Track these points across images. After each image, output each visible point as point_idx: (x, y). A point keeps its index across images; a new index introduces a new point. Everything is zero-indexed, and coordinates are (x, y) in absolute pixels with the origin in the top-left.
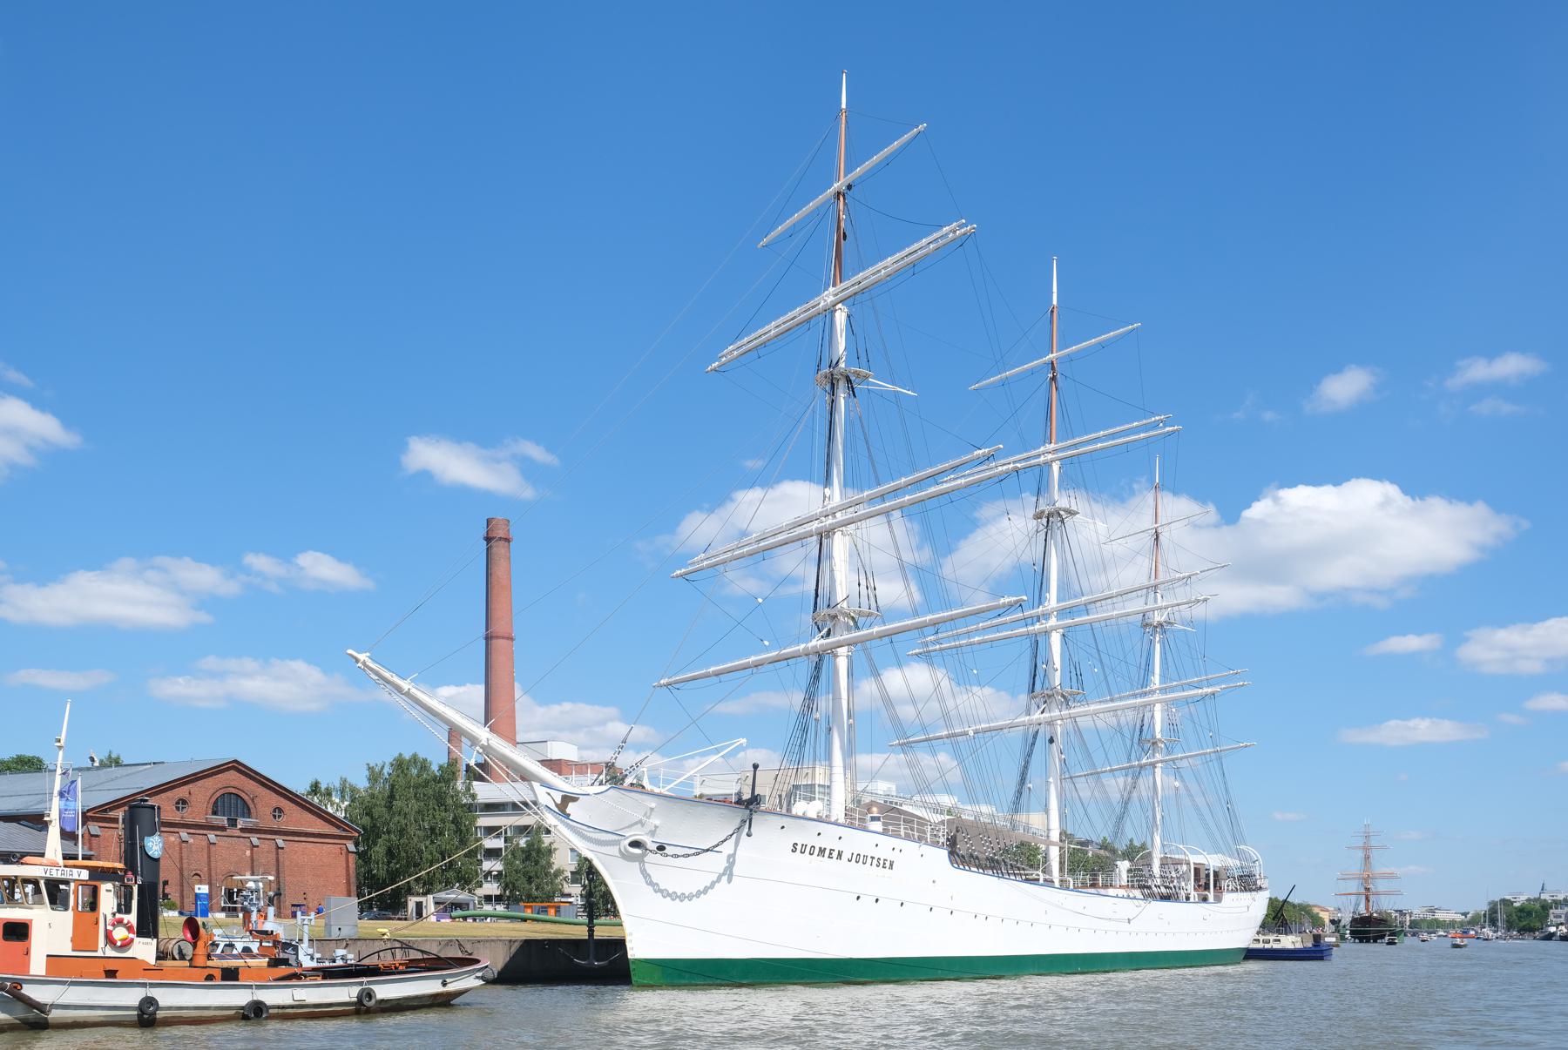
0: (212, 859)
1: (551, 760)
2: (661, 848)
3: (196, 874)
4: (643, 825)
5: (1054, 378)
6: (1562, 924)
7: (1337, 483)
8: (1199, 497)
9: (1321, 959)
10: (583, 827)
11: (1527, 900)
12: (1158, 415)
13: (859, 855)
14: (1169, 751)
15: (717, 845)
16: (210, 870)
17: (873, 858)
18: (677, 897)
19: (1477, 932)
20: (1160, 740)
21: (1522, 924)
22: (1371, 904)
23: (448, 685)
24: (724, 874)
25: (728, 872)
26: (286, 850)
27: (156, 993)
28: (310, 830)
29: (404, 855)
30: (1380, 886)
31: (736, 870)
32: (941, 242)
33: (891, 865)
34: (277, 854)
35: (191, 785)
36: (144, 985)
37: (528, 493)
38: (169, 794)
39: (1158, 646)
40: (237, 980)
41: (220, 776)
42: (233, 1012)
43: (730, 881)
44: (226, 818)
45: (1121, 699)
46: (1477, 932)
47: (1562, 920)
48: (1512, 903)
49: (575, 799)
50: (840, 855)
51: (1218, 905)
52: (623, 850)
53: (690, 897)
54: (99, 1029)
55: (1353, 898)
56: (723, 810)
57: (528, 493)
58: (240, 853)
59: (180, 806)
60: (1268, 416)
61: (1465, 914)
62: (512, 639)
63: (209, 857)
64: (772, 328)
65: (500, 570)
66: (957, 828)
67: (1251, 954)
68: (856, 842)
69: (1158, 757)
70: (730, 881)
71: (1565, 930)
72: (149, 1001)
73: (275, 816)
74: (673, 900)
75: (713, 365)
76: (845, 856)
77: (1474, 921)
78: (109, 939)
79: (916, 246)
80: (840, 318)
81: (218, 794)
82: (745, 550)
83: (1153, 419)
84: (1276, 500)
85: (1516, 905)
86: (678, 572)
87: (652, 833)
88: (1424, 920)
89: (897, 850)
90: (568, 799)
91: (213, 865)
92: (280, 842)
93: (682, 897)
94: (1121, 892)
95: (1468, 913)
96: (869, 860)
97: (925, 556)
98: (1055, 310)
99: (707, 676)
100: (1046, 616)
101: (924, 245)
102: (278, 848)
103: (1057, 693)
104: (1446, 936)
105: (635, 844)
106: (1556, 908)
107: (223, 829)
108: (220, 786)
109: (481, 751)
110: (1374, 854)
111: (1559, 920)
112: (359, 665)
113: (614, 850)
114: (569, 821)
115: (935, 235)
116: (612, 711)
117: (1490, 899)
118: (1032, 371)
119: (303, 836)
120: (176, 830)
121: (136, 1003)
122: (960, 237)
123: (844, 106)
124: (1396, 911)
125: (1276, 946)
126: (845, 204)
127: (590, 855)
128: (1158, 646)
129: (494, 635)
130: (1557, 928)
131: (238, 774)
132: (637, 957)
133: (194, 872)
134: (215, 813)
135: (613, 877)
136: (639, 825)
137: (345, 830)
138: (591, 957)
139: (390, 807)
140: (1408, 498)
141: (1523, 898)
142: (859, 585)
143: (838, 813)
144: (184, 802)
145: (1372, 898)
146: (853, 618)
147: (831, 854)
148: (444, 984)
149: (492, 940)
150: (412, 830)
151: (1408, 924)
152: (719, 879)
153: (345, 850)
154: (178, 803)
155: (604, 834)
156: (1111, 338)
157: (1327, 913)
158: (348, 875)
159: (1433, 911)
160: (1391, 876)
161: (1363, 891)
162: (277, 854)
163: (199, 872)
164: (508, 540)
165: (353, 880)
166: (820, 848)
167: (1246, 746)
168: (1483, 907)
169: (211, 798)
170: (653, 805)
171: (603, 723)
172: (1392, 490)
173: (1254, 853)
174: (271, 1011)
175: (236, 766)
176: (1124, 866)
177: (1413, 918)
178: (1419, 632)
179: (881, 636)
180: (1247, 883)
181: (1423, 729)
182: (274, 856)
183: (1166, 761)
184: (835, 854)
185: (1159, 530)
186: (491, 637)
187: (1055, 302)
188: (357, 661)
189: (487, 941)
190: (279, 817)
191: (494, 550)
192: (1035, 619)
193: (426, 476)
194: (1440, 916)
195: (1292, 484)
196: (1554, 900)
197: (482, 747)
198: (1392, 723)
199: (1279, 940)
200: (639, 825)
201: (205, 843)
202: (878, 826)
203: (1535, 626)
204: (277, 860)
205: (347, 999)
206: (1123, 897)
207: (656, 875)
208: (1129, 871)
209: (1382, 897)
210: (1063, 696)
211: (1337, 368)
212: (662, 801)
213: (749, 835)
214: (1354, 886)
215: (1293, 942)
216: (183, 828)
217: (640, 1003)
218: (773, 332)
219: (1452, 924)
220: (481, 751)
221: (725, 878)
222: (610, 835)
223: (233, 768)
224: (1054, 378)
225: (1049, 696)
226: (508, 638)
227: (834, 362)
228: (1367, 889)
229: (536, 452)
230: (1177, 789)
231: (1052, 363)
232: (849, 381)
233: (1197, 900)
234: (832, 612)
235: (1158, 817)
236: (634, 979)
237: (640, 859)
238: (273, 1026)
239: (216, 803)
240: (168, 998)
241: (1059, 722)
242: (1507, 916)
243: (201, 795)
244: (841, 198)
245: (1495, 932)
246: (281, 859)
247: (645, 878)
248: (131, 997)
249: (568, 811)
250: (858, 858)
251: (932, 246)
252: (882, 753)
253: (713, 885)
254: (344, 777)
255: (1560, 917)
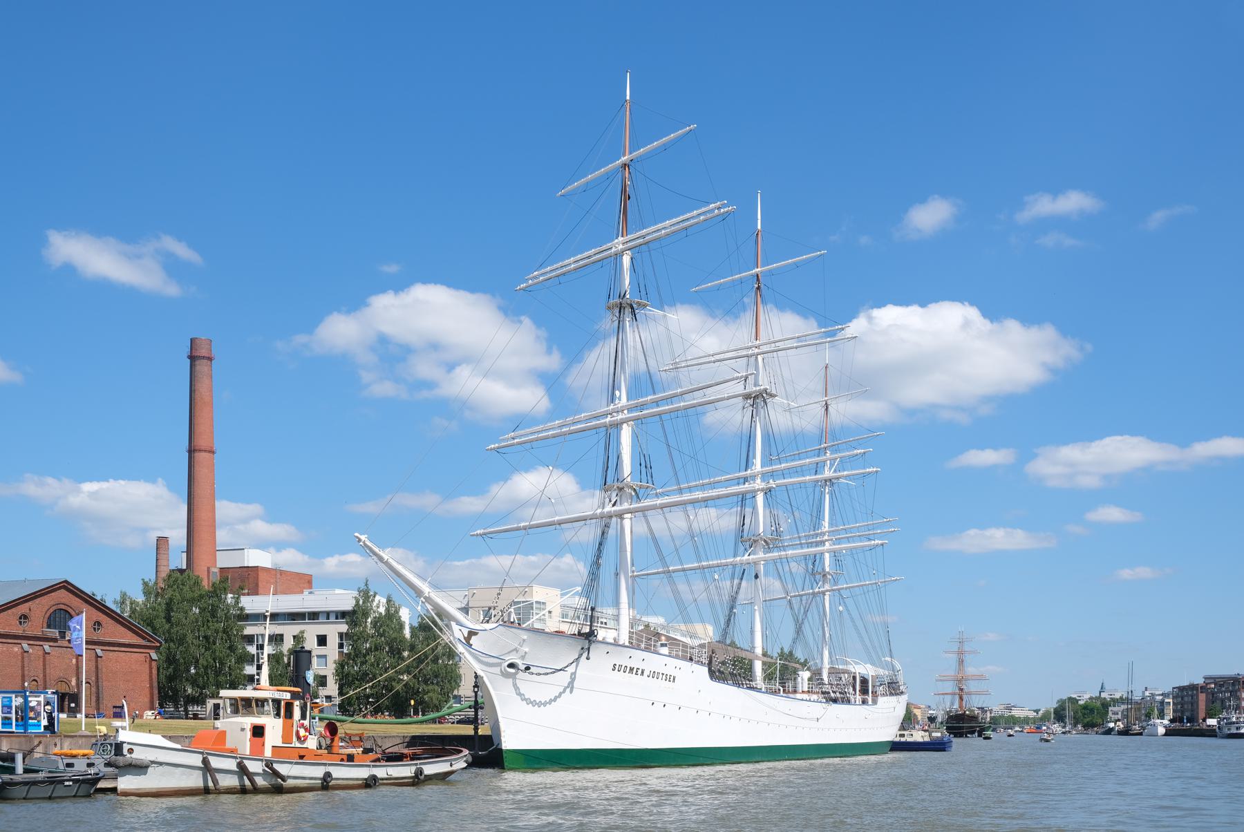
0: (47, 666)
1: (248, 567)
2: (528, 668)
3: (34, 680)
4: (517, 651)
5: (758, 288)
6: (1119, 720)
7: (923, 304)
8: (803, 310)
9: (944, 750)
10: (477, 653)
11: (1090, 699)
12: (840, 325)
13: (626, 666)
14: (836, 583)
15: (565, 667)
16: (45, 676)
17: (663, 674)
18: (536, 704)
19: (1048, 728)
20: (829, 573)
21: (1086, 720)
22: (964, 703)
23: (91, 481)
24: (568, 687)
25: (571, 685)
26: (53, 653)
27: (331, 769)
28: (122, 641)
29: (183, 661)
30: (971, 686)
31: (576, 684)
32: (709, 216)
33: (674, 679)
34: (97, 662)
35: (30, 603)
36: (325, 765)
37: (173, 290)
38: (14, 610)
39: (827, 496)
40: (353, 761)
41: (53, 594)
42: (361, 782)
43: (571, 692)
44: (57, 631)
45: (690, 489)
46: (1048, 728)
47: (1119, 716)
48: (1077, 701)
49: (476, 634)
50: (643, 672)
51: (875, 706)
52: (503, 669)
53: (545, 704)
54: (385, 786)
55: (948, 698)
56: (571, 641)
57: (173, 290)
58: (67, 661)
59: (22, 620)
60: (864, 240)
61: (1037, 711)
62: (213, 452)
63: (44, 665)
64: (571, 262)
65: (202, 388)
66: (712, 650)
67: (896, 747)
68: (638, 658)
69: (827, 587)
70: (571, 692)
71: (1122, 726)
72: (328, 775)
73: (95, 629)
74: (528, 704)
75: (522, 286)
76: (646, 673)
77: (1045, 718)
78: (299, 738)
79: (688, 215)
80: (626, 260)
81: (51, 610)
82: (550, 433)
83: (837, 327)
84: (870, 319)
85: (1081, 703)
86: (493, 446)
87: (523, 658)
88: (1002, 717)
89: (678, 668)
90: (472, 633)
91: (48, 671)
92: (99, 652)
93: (540, 704)
94: (805, 696)
95: (1039, 710)
96: (661, 675)
97: (552, 362)
98: (759, 233)
99: (518, 529)
100: (753, 477)
101: (695, 215)
102: (97, 657)
103: (761, 538)
104: (1022, 731)
105: (511, 666)
106: (1114, 706)
107: (55, 640)
108: (52, 603)
109: (424, 600)
110: (968, 658)
111: (1116, 717)
112: (361, 543)
113: (497, 670)
114: (471, 650)
115: (704, 209)
116: (255, 508)
117: (1058, 698)
118: (741, 281)
119: (117, 646)
120: (19, 641)
121: (322, 776)
122: (724, 213)
123: (628, 98)
124: (978, 708)
125: (909, 740)
126: (630, 173)
127: (480, 673)
128: (827, 496)
129: (197, 448)
130: (1115, 724)
131: (67, 593)
132: (508, 748)
133: (32, 678)
134: (49, 627)
135: (494, 688)
136: (515, 652)
137: (149, 641)
138: (476, 748)
139: (168, 619)
140: (987, 322)
141: (1087, 696)
142: (641, 465)
143: (624, 639)
144: (25, 617)
145: (965, 697)
146: (635, 490)
147: (637, 671)
148: (451, 766)
149: (393, 737)
150: (189, 638)
151: (988, 720)
152: (564, 691)
153: (149, 659)
154: (20, 618)
155: (492, 659)
156: (803, 260)
157: (920, 710)
158: (151, 679)
159: (1009, 708)
160: (980, 678)
161: (957, 691)
162: (97, 662)
163: (36, 678)
164: (210, 359)
165: (155, 684)
166: (630, 668)
167: (896, 580)
168: (1052, 705)
169: (46, 612)
170: (525, 637)
171: (245, 521)
172: (972, 313)
173: (898, 666)
174: (380, 781)
175: (66, 586)
176: (805, 675)
177: (992, 715)
178: (995, 447)
179: (846, 588)
180: (893, 688)
181: (999, 538)
182: (94, 663)
183: (833, 590)
184: (640, 672)
185: (829, 402)
186: (194, 450)
187: (759, 227)
188: (360, 540)
189: (390, 737)
190: (99, 629)
191: (198, 368)
192: (742, 480)
193: (69, 270)
194: (1016, 713)
195: (881, 304)
196: (1111, 698)
197: (425, 598)
198: (972, 532)
199: (912, 735)
200: (515, 652)
201: (41, 653)
202: (665, 650)
203: (1093, 444)
204: (97, 667)
205: (409, 775)
206: (806, 700)
207: (523, 689)
208: (810, 679)
209: (973, 696)
210: (765, 541)
211: (923, 200)
212: (530, 634)
213: (588, 658)
214: (950, 687)
215: (922, 737)
216: (24, 640)
217: (513, 779)
218: (573, 266)
219: (1026, 721)
220: (424, 600)
221: (568, 690)
222: (495, 659)
223: (64, 587)
224: (758, 288)
225: (755, 541)
226: (209, 452)
227: (622, 295)
228: (961, 690)
229: (181, 250)
230: (841, 612)
231: (757, 275)
232: (632, 308)
233: (861, 703)
234: (621, 485)
235: (827, 635)
236: (506, 764)
237: (513, 676)
238: (384, 789)
239: (49, 618)
240: (341, 773)
241: (762, 562)
242: (1074, 713)
243: (39, 610)
244: (627, 169)
245: (1064, 727)
246: (100, 667)
247: (516, 690)
248: (319, 772)
249: (471, 642)
250: (654, 675)
251: (702, 218)
252: (510, 555)
253: (560, 694)
254: (123, 591)
255: (1117, 714)
